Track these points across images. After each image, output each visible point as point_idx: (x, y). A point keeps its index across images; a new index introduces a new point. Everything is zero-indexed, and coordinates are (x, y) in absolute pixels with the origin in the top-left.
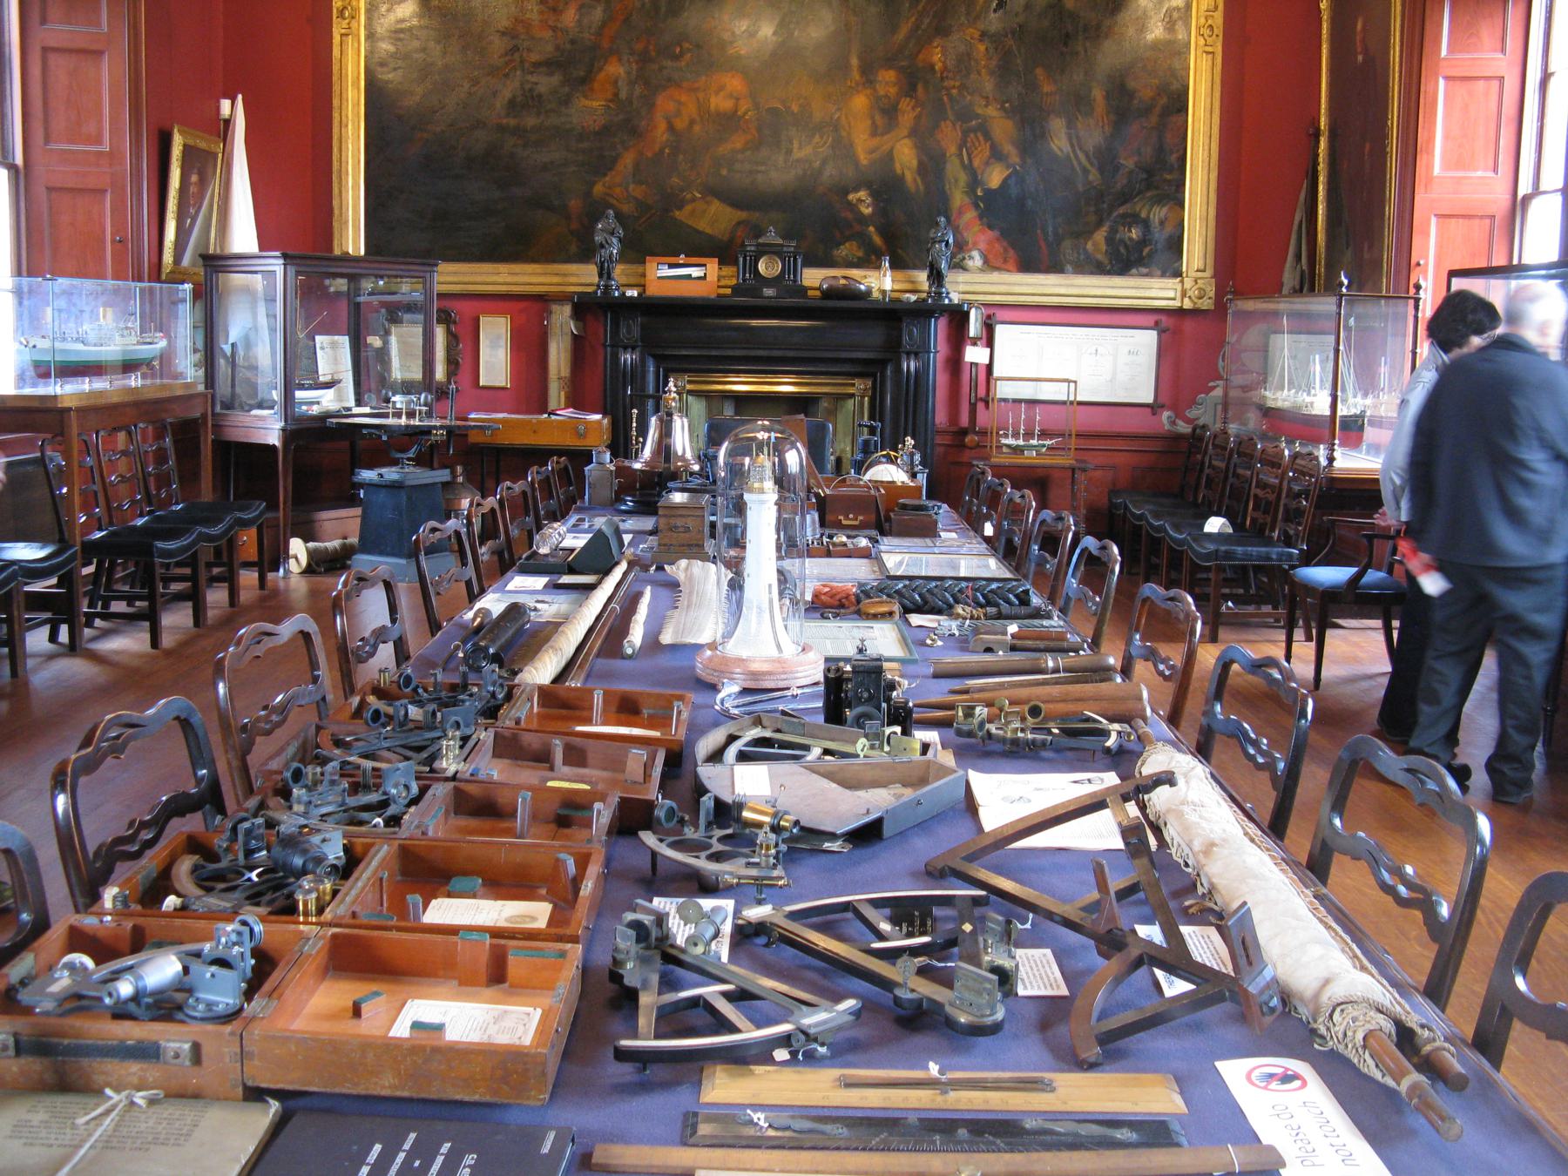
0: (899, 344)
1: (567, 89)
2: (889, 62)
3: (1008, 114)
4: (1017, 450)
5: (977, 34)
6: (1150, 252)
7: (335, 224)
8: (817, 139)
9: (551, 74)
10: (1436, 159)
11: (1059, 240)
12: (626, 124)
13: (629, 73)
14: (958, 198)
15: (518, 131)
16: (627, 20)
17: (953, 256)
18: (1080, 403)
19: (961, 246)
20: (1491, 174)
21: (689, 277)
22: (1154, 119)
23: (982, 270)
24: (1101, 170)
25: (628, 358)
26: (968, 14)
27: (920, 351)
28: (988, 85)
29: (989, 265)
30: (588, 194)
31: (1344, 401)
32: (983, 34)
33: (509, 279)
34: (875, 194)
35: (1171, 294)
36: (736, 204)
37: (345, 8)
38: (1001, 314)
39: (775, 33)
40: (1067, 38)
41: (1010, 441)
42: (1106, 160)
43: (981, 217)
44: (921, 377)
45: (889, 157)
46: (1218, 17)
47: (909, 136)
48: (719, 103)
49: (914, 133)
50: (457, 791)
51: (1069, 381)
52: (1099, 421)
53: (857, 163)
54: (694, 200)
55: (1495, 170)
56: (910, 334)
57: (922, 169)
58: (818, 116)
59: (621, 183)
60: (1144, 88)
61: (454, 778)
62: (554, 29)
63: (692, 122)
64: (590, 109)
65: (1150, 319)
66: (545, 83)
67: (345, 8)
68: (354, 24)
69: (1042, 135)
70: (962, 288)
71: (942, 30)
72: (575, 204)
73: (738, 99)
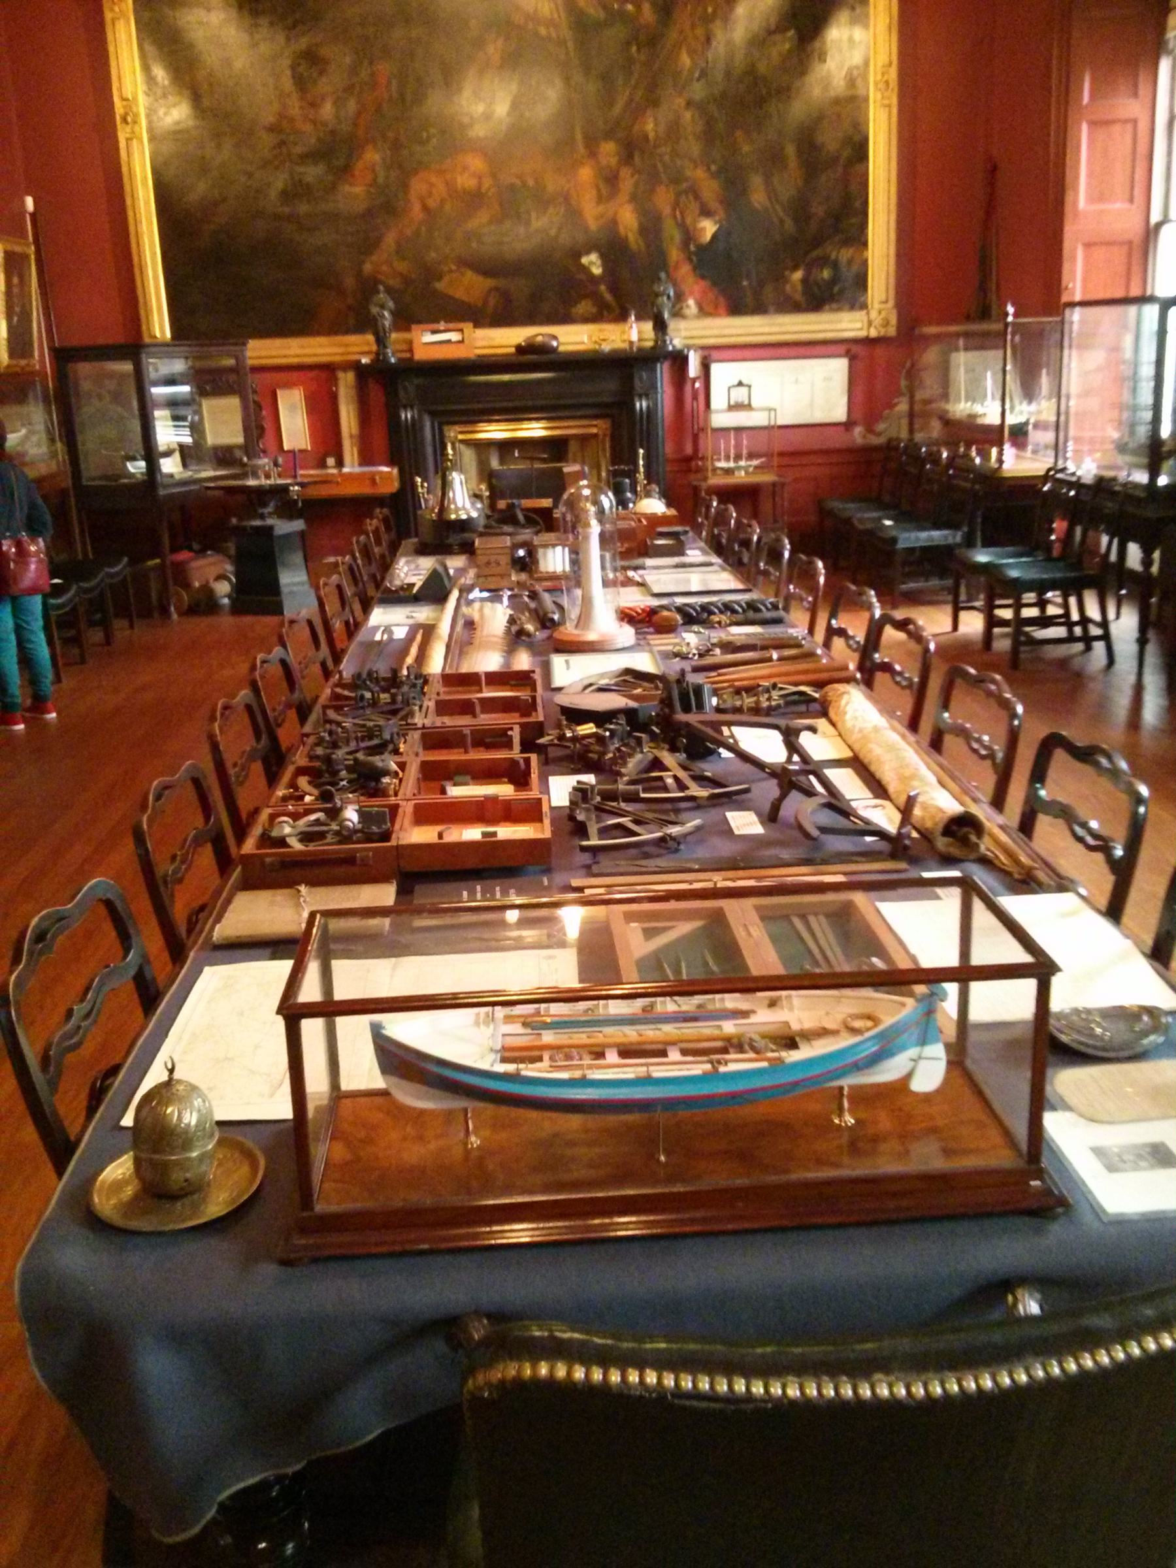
0: (632, 388)
1: (330, 178)
2: (609, 135)
3: (714, 176)
4: (728, 472)
5: (683, 104)
6: (836, 290)
7: (142, 312)
8: (551, 210)
9: (316, 164)
10: (1082, 196)
11: (761, 284)
12: (387, 205)
13: (383, 159)
14: (674, 254)
15: (289, 218)
16: (379, 109)
17: (673, 306)
18: (781, 427)
19: (680, 297)
20: (1127, 205)
21: (449, 341)
22: (840, 169)
23: (698, 317)
24: (796, 220)
25: (407, 415)
26: (675, 86)
27: (649, 392)
28: (695, 149)
29: (703, 312)
30: (359, 273)
31: (1012, 408)
32: (689, 104)
33: (299, 352)
34: (603, 256)
35: (859, 325)
36: (486, 273)
37: (126, 114)
38: (715, 354)
39: (509, 114)
40: (761, 101)
41: (722, 464)
42: (800, 210)
43: (695, 269)
44: (651, 413)
45: (614, 222)
46: (893, 74)
47: (630, 202)
48: (465, 181)
49: (633, 198)
50: (423, 735)
51: (770, 410)
52: (797, 441)
53: (587, 230)
54: (451, 271)
55: (1131, 200)
56: (641, 378)
57: (643, 230)
58: (551, 187)
59: (385, 261)
60: (830, 140)
61: (424, 727)
62: (314, 122)
63: (443, 201)
64: (354, 194)
65: (842, 349)
66: (313, 173)
67: (126, 114)
68: (137, 128)
69: (744, 192)
70: (684, 334)
71: (653, 102)
72: (349, 282)
73: (480, 178)
